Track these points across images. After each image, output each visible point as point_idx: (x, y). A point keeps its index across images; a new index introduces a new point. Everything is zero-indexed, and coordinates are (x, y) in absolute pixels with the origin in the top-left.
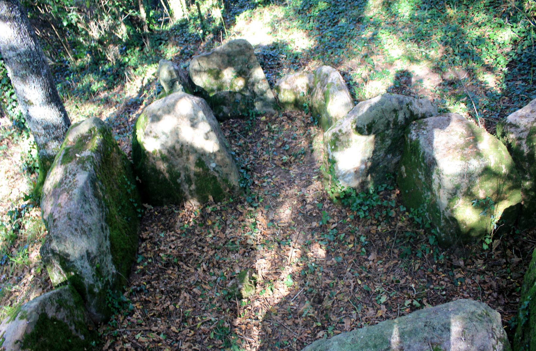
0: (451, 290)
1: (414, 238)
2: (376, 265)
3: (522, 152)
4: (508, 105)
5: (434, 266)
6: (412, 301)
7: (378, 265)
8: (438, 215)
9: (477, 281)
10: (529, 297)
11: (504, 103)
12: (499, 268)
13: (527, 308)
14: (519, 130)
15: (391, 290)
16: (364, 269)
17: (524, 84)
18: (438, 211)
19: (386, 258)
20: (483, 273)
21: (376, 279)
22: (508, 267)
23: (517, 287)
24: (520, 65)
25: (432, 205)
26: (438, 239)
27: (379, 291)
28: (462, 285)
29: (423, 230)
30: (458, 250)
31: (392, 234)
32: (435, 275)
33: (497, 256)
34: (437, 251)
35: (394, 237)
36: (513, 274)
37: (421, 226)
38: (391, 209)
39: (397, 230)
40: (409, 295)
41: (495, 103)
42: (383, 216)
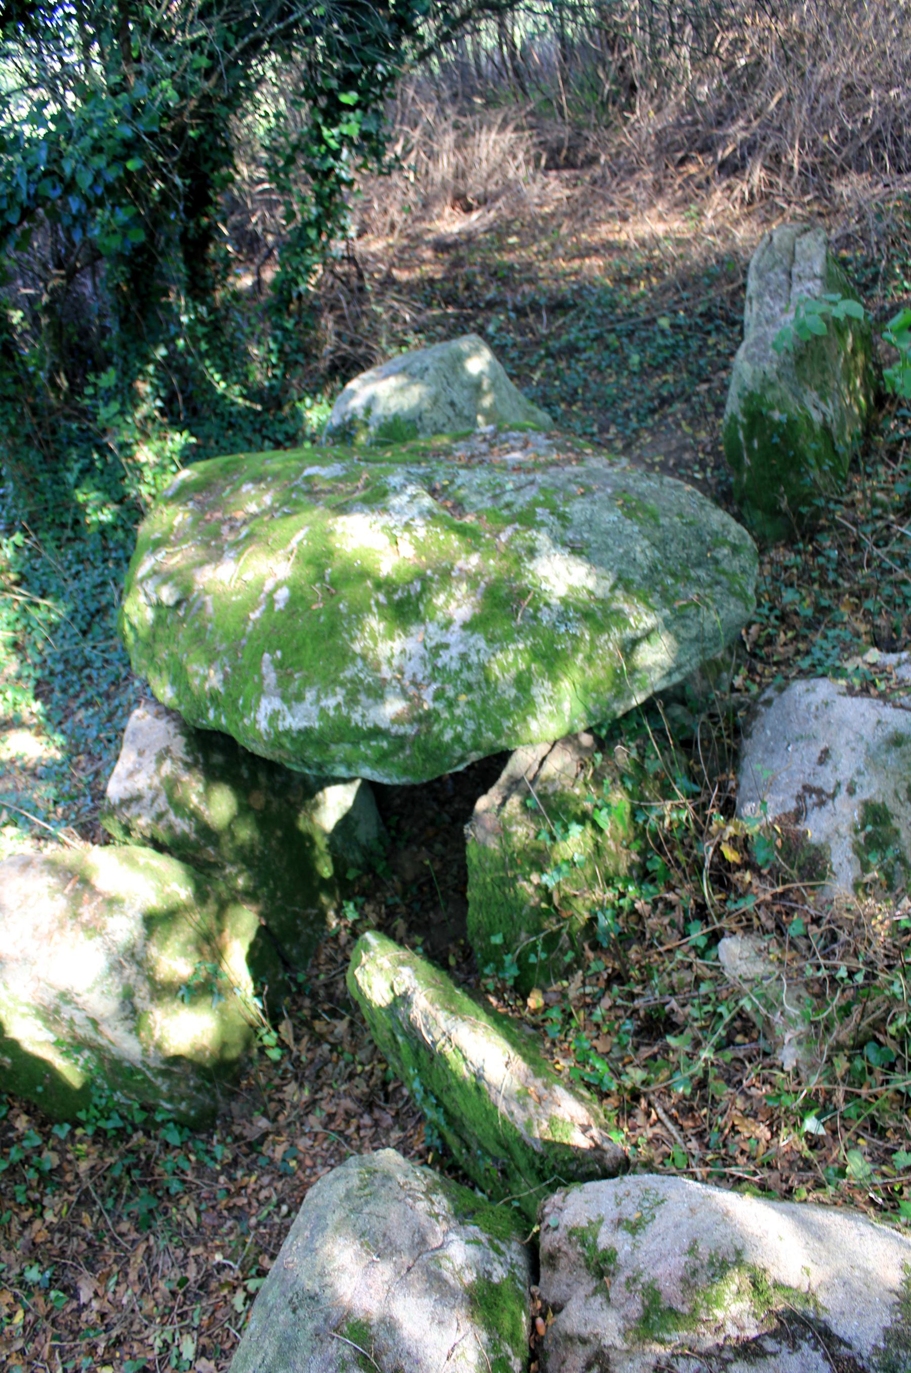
0: (293, 1190)
1: (136, 1166)
2: (110, 1295)
3: (185, 836)
4: (94, 768)
5: (222, 1179)
6: (245, 1289)
7: (115, 1292)
8: (139, 1077)
9: (318, 1128)
10: (411, 1072)
11: (83, 770)
12: (329, 1068)
13: (425, 1091)
14: (146, 801)
15: (186, 1312)
16: (92, 1333)
17: (91, 711)
18: (133, 1071)
19: (116, 1261)
20: (313, 1103)
21: (136, 1327)
22: (341, 1053)
23: (385, 1071)
24: (57, 683)
25: (111, 1070)
26: (181, 1123)
27: (165, 1341)
28: (300, 1163)
29: (141, 1133)
30: (235, 1107)
31: (85, 1200)
32: (238, 1194)
33: (309, 1050)
34: (201, 1146)
35: (95, 1203)
36: (361, 1056)
37: (129, 1129)
38: (40, 1154)
39: (88, 1183)
40: (227, 1283)
41: (67, 782)
42: (35, 1184)
